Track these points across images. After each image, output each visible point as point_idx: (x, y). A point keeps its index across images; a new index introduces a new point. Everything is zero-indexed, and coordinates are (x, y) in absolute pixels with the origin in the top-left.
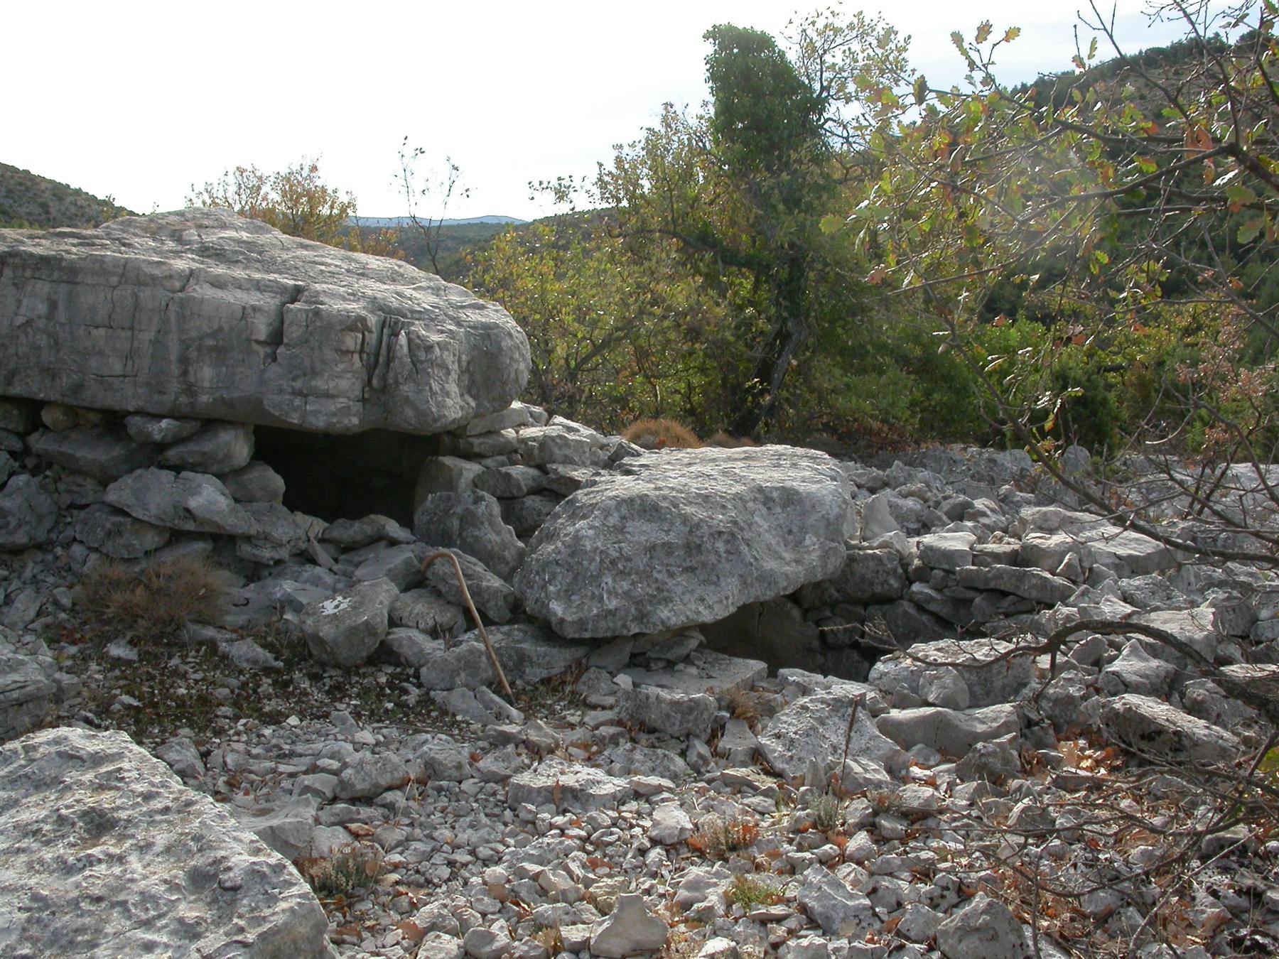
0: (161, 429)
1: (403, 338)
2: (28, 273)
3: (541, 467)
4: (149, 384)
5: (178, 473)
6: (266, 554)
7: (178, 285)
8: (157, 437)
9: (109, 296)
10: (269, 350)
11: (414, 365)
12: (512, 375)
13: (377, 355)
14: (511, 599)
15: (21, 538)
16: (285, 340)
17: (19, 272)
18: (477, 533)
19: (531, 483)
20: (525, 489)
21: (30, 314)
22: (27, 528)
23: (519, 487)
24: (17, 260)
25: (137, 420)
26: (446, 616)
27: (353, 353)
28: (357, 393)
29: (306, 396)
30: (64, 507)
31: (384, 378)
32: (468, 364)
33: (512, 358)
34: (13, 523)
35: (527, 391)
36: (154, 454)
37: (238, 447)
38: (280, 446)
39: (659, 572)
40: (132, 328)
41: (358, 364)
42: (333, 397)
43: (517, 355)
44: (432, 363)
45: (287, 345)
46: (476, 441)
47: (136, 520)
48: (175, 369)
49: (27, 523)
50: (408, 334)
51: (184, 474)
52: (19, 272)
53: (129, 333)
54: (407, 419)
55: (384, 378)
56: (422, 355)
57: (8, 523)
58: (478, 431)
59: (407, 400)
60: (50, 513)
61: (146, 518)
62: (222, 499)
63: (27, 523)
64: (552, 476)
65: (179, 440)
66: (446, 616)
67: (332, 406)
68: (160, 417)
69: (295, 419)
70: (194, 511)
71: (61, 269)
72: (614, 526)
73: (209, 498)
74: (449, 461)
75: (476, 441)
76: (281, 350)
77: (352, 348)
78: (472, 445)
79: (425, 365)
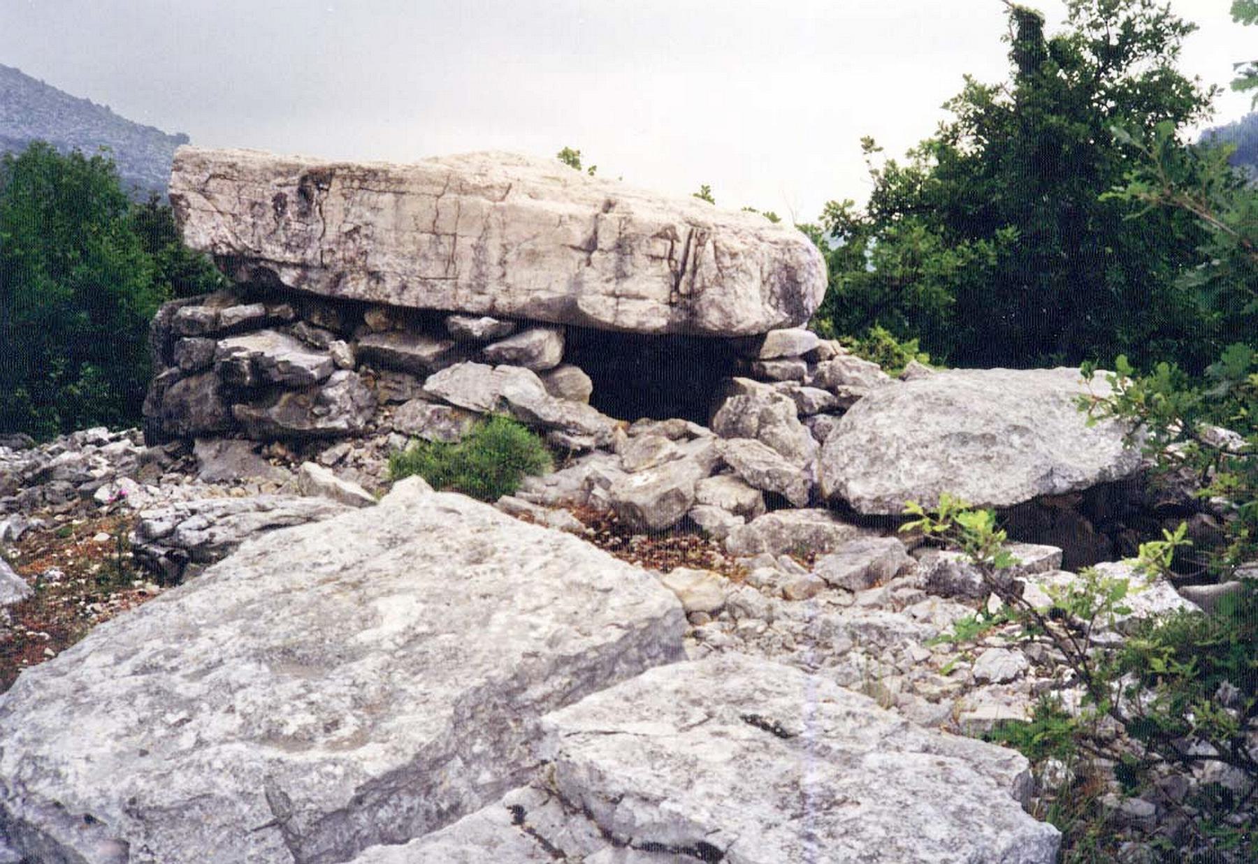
0: (477, 327)
1: (709, 246)
2: (356, 184)
3: (832, 389)
4: (470, 286)
5: (494, 367)
6: (577, 442)
7: (498, 194)
8: (478, 334)
9: (434, 204)
10: (583, 255)
11: (720, 270)
12: (810, 289)
13: (684, 264)
14: (809, 484)
15: (341, 424)
16: (600, 246)
17: (347, 183)
18: (775, 430)
19: (822, 402)
20: (817, 407)
21: (358, 222)
22: (348, 416)
23: (811, 406)
24: (345, 172)
25: (457, 319)
26: (748, 497)
27: (662, 258)
28: (666, 296)
29: (618, 297)
30: (383, 402)
31: (691, 283)
32: (770, 275)
33: (810, 273)
34: (334, 408)
35: (819, 315)
36: (472, 349)
37: (550, 346)
38: (589, 343)
39: (956, 458)
40: (454, 235)
41: (667, 270)
42: (643, 298)
43: (814, 271)
44: (738, 269)
45: (601, 250)
46: (768, 365)
47: (456, 407)
48: (496, 271)
49: (348, 412)
50: (714, 243)
51: (500, 367)
52: (347, 183)
53: (452, 239)
54: (712, 320)
55: (691, 283)
56: (727, 261)
57: (329, 411)
58: (770, 355)
59: (712, 302)
60: (369, 407)
61: (464, 405)
62: (535, 389)
63: (348, 412)
64: (843, 395)
65: (495, 338)
66: (748, 497)
67: (641, 306)
68: (478, 316)
69: (607, 317)
70: (510, 399)
71: (388, 180)
72: (910, 417)
73: (522, 386)
74: (743, 381)
75: (768, 365)
76: (596, 255)
77: (662, 255)
78: (764, 368)
79: (731, 271)
